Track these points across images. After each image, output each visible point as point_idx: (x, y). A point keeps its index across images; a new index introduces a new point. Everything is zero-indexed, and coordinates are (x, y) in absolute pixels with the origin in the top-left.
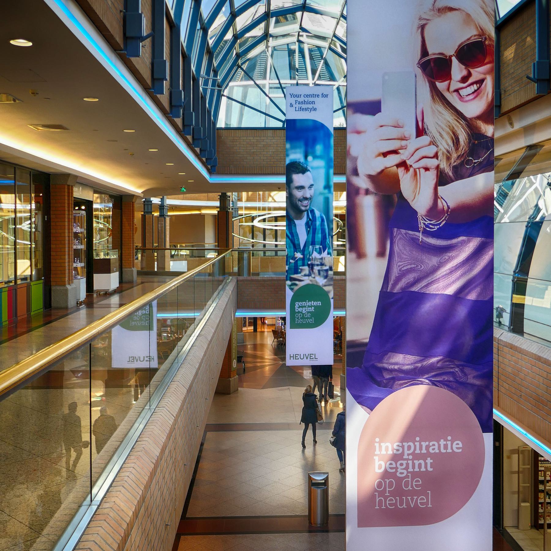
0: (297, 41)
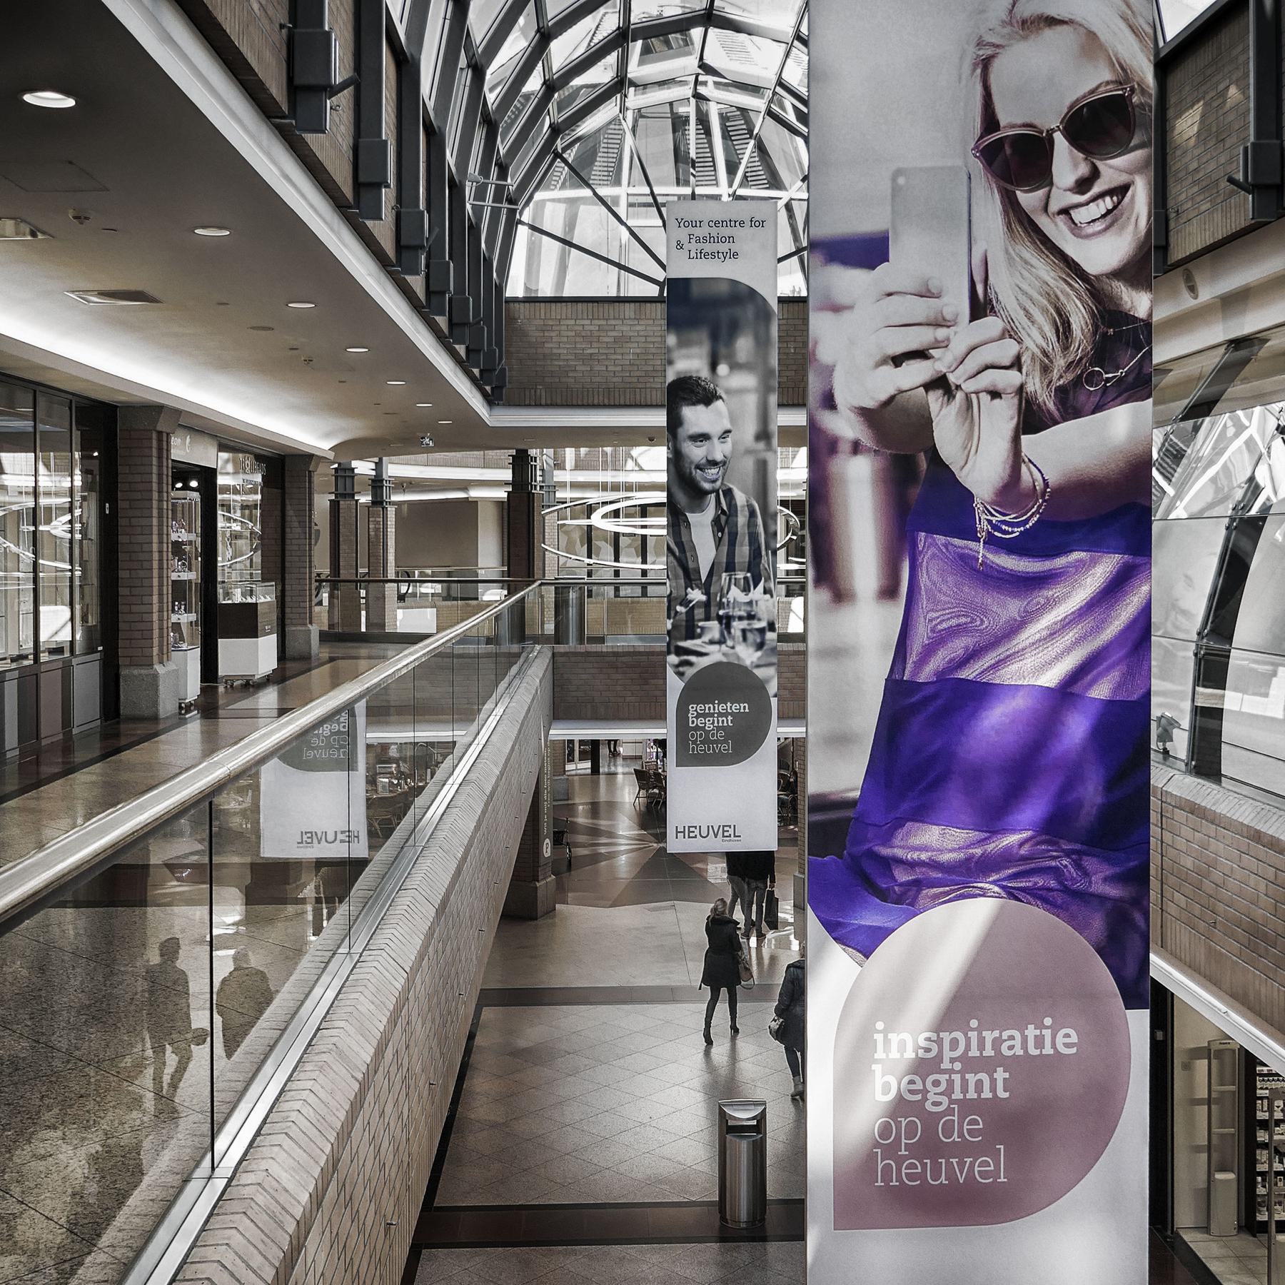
0: (694, 96)
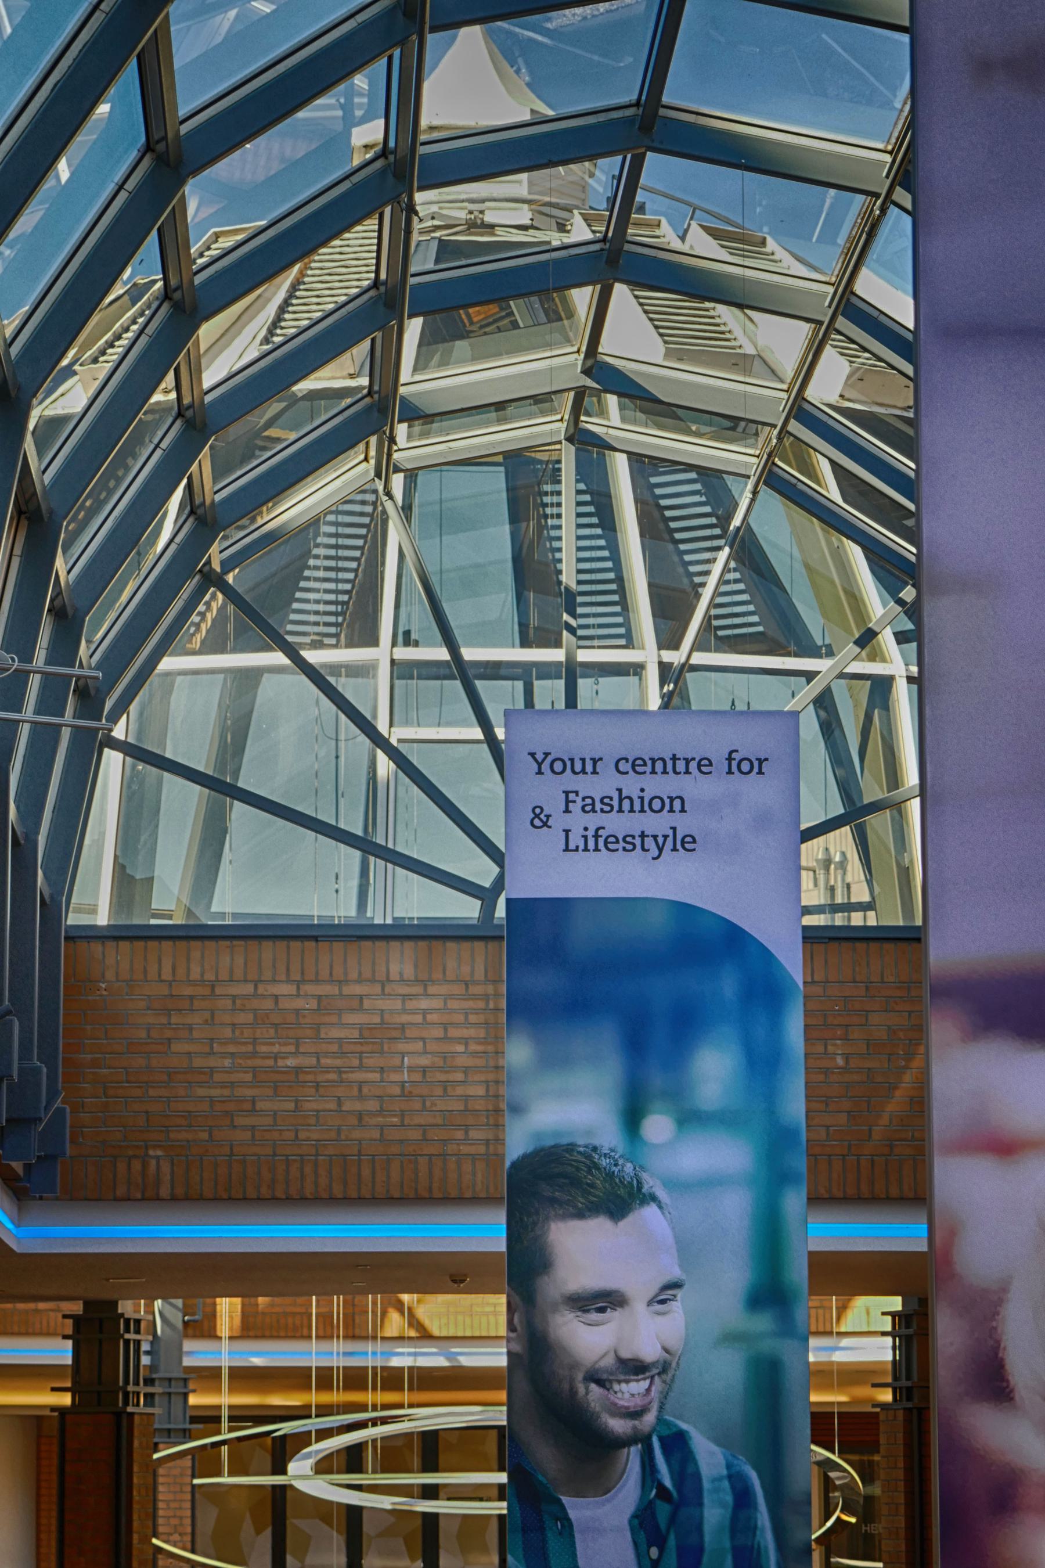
0: (570, 439)
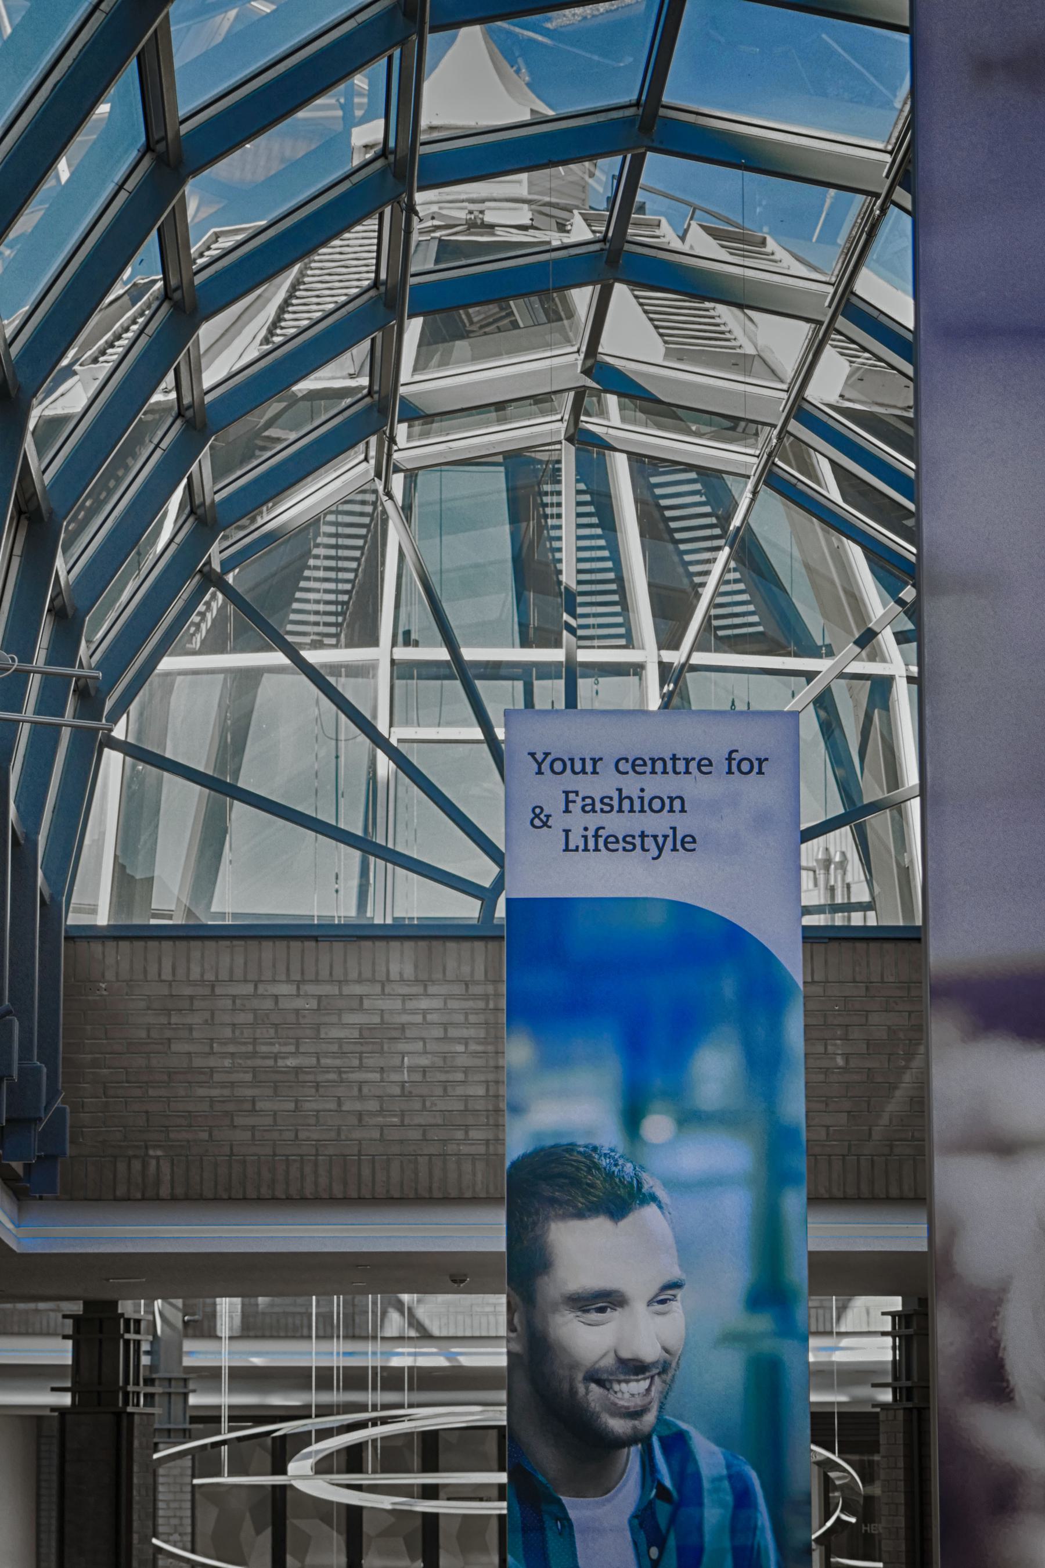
0: (570, 439)
